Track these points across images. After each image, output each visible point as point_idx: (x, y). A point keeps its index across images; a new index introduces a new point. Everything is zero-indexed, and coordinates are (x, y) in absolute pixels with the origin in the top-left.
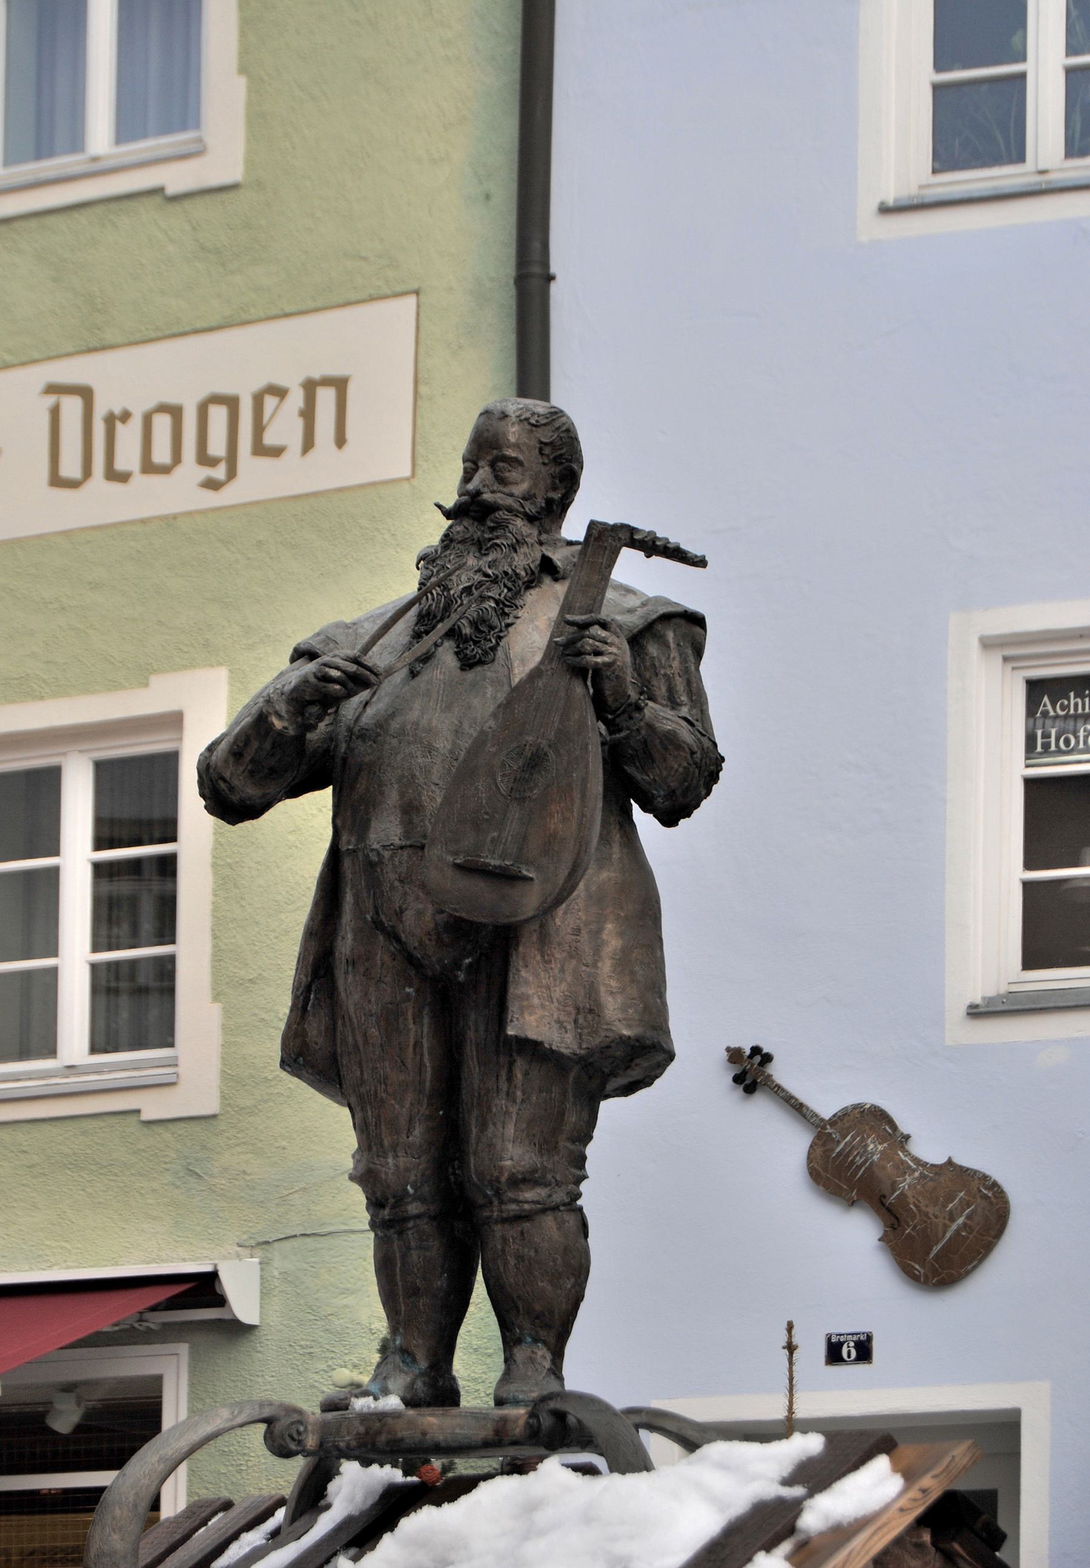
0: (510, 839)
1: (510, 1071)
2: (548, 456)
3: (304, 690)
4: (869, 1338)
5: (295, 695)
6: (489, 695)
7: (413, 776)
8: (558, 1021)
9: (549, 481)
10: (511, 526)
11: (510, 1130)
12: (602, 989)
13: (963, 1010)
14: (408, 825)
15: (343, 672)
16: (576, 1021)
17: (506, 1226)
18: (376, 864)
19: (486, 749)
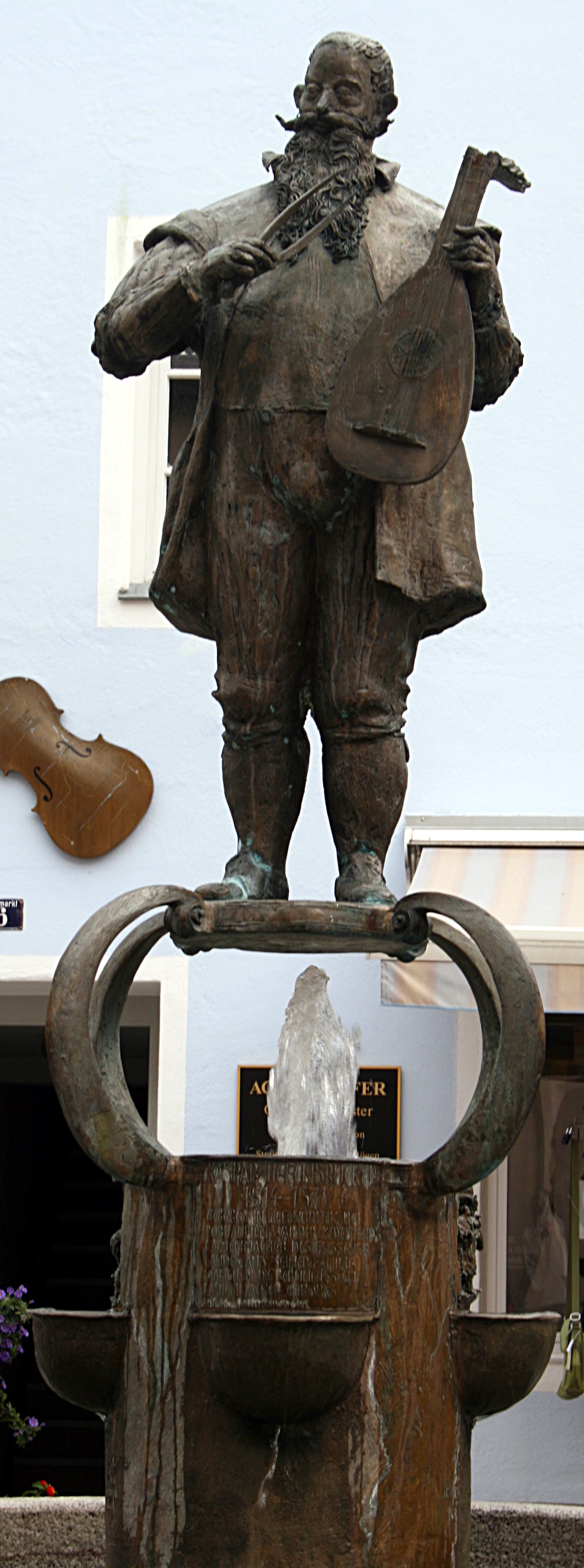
0: (402, 411)
1: (369, 612)
2: (377, 85)
3: (220, 270)
4: (20, 905)
5: (210, 272)
6: (357, 286)
7: (301, 351)
8: (410, 572)
9: (375, 106)
10: (354, 143)
11: (367, 664)
12: (443, 546)
13: (115, 595)
14: (298, 393)
15: (255, 257)
16: (422, 572)
17: (354, 746)
18: (267, 424)
19: (381, 333)
